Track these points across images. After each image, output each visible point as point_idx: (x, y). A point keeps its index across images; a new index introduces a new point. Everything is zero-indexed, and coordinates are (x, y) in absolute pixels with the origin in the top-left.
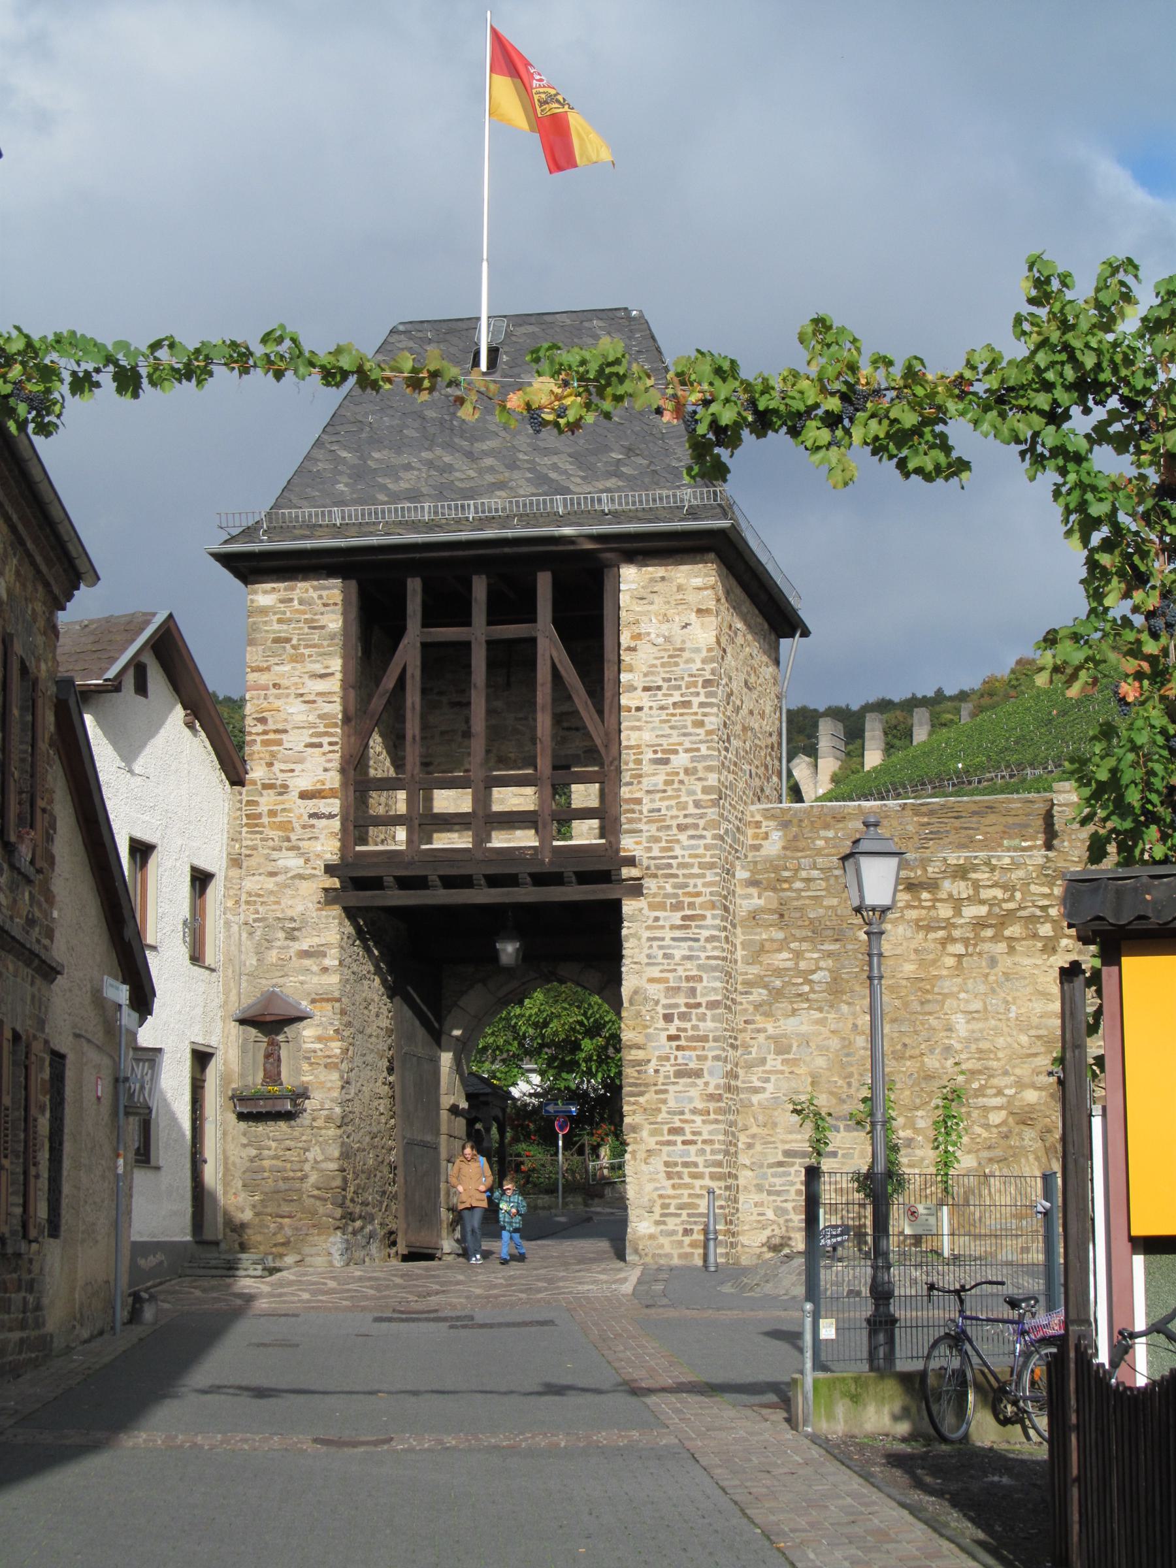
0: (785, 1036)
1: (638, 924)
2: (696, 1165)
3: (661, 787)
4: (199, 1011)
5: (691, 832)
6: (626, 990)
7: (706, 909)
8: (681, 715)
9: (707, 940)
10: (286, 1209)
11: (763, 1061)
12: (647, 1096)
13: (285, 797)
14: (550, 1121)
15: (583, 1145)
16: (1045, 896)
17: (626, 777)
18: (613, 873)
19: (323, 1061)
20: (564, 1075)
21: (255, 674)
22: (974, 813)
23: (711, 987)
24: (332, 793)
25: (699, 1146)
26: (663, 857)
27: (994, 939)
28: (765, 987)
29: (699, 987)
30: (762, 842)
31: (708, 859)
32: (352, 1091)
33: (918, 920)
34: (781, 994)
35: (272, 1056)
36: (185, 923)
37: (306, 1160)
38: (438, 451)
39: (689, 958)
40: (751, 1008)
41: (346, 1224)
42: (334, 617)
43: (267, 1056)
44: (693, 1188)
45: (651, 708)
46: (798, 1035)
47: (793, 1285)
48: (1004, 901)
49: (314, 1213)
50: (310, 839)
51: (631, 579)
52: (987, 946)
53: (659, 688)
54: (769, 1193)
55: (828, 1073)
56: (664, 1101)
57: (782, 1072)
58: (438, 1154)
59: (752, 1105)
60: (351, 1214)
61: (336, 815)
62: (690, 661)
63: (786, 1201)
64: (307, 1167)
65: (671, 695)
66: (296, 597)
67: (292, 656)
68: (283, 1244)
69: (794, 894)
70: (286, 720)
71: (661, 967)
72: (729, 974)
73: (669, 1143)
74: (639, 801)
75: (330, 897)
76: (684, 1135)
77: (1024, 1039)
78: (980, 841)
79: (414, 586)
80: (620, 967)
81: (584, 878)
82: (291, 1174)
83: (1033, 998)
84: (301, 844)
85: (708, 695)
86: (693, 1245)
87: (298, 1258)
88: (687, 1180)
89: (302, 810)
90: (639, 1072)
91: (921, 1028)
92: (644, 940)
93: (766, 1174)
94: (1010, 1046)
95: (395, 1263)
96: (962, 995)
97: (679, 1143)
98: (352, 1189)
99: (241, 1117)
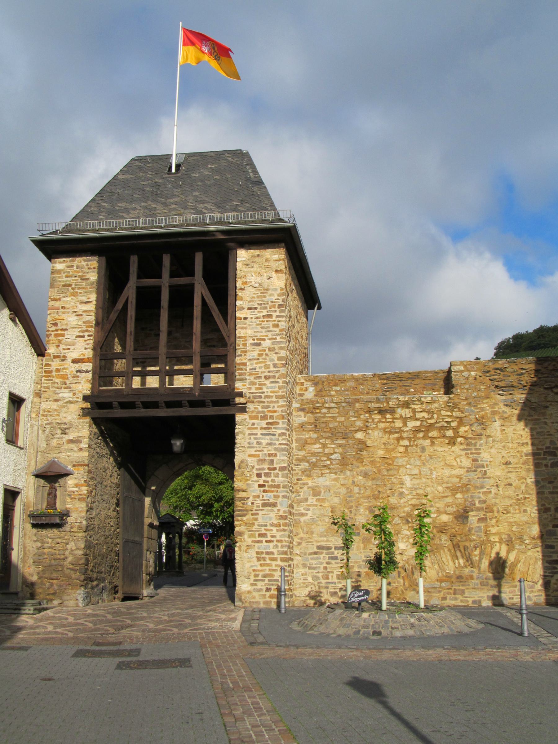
0: (317, 487)
1: (244, 426)
2: (273, 553)
3: (256, 357)
4: (11, 468)
5: (272, 380)
6: (237, 461)
7: (279, 419)
8: (267, 321)
9: (280, 435)
10: (55, 575)
11: (306, 500)
12: (247, 517)
13: (65, 362)
14: (201, 535)
15: (214, 545)
16: (449, 416)
17: (238, 352)
18: (231, 400)
19: (78, 497)
20: (207, 517)
21: (53, 302)
22: (409, 378)
23: (281, 459)
24: (88, 360)
25: (275, 543)
26: (257, 393)
27: (424, 438)
28: (308, 461)
29: (275, 459)
30: (305, 393)
31: (280, 394)
32: (94, 513)
33: (385, 428)
34: (315, 466)
35: (52, 496)
36: (3, 421)
37: (67, 549)
38: (150, 203)
39: (270, 444)
40: (300, 473)
41: (87, 583)
42: (94, 274)
43: (49, 494)
44: (271, 566)
45: (252, 318)
46: (324, 486)
47: (338, 627)
48: (428, 419)
49: (69, 577)
50: (76, 383)
51: (243, 255)
52: (420, 442)
53: (256, 308)
54: (310, 568)
55: (339, 506)
56: (256, 519)
57: (316, 505)
58: (143, 547)
59: (301, 522)
60: (90, 578)
61: (90, 371)
62: (272, 295)
63: (318, 572)
64: (67, 553)
65: (262, 312)
66: (75, 265)
67: (71, 293)
68: (52, 594)
69: (322, 415)
70: (67, 324)
71: (255, 449)
72: (289, 453)
73: (259, 542)
74: (245, 364)
75: (85, 412)
76: (267, 537)
77: (440, 489)
78: (412, 392)
79: (134, 260)
80: (234, 449)
81: (216, 403)
82: (59, 556)
83: (445, 468)
84: (71, 385)
85: (281, 312)
86: (271, 597)
87: (60, 601)
88: (268, 561)
89: (73, 369)
90: (243, 504)
91: (387, 483)
92: (246, 435)
93: (307, 558)
94: (433, 492)
95: (117, 602)
96: (408, 466)
97: (264, 541)
98: (92, 565)
99: (34, 526)
